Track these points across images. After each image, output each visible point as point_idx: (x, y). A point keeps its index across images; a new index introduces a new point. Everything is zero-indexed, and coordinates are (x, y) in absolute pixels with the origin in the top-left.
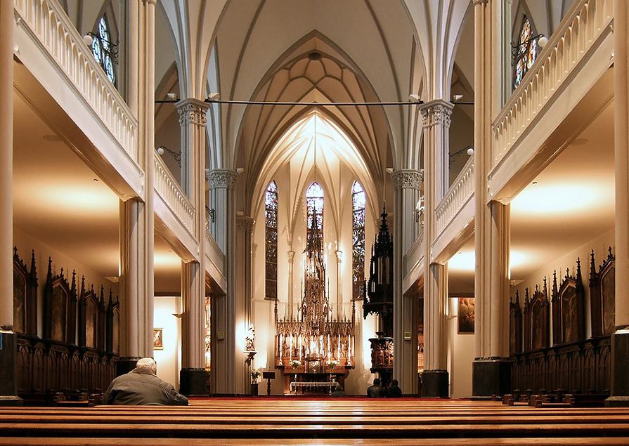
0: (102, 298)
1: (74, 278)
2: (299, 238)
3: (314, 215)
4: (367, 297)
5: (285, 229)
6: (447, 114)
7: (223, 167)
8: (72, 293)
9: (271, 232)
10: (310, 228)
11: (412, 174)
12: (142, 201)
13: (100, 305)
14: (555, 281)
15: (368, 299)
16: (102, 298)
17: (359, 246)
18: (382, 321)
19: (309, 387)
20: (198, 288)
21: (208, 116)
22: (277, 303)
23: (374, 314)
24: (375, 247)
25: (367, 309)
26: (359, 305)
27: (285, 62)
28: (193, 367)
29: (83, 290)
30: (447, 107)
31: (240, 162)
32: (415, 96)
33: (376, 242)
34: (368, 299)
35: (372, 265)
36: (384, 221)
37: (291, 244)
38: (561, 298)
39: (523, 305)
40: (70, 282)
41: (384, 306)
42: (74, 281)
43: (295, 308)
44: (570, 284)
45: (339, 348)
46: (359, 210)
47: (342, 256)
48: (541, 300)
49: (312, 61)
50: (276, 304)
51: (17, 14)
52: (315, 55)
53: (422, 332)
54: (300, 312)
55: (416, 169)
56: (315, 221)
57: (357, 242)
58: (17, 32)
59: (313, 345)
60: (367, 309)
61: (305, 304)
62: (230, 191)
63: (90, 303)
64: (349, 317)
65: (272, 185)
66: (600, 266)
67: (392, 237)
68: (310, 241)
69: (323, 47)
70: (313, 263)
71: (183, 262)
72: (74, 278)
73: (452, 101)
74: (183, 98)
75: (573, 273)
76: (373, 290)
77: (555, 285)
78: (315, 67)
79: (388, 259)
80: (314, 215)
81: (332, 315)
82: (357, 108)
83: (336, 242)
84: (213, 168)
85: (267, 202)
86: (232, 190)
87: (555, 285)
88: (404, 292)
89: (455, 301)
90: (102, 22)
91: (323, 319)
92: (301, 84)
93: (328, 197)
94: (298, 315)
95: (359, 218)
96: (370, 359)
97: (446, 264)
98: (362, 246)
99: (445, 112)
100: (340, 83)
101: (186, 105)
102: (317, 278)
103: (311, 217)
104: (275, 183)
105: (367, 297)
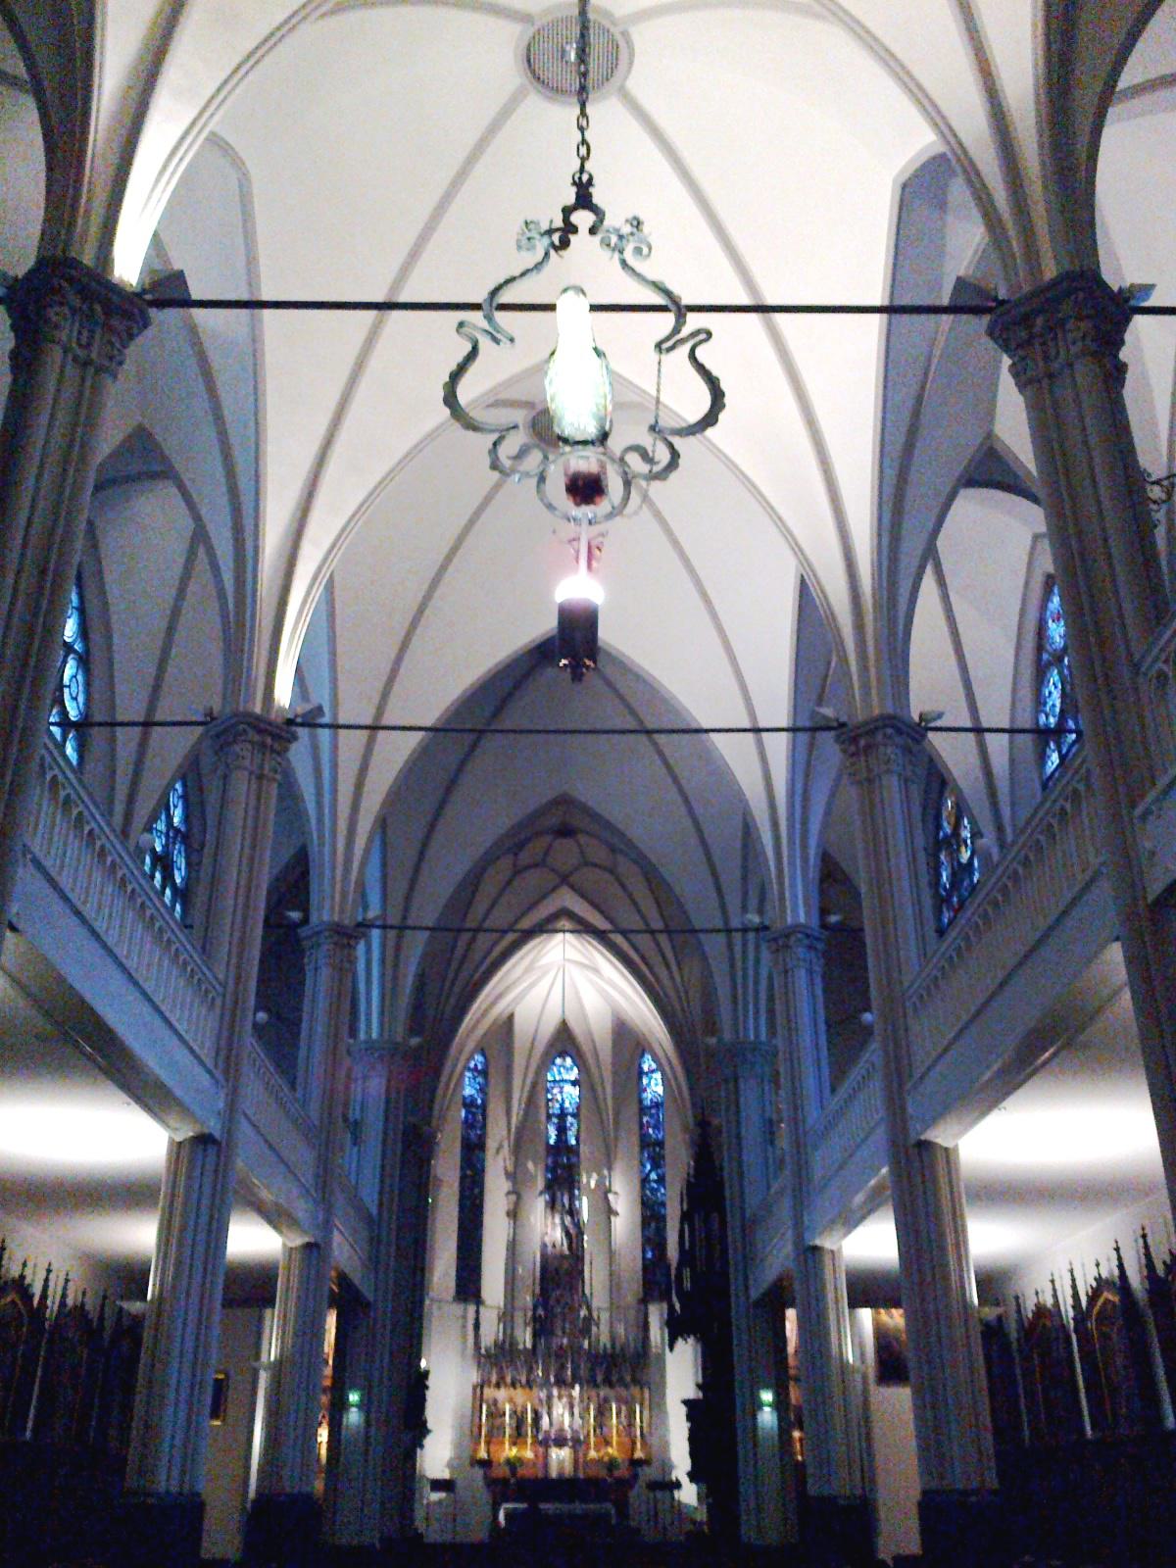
1: (47, 1280)
2: (530, 1165)
4: (675, 1299)
9: (473, 1151)
10: (552, 1142)
14: (1074, 1287)
15: (677, 1306)
21: (361, 947)
23: (691, 1340)
25: (676, 1329)
26: (656, 1315)
27: (514, 842)
29: (63, 1304)
31: (415, 1028)
32: (754, 918)
34: (677, 1306)
37: (511, 1176)
38: (1091, 1325)
40: (37, 1290)
43: (519, 1319)
44: (1107, 1295)
49: (558, 841)
50: (477, 1312)
51: (26, 849)
52: (566, 832)
55: (763, 1037)
56: (562, 1130)
58: (25, 879)
59: (560, 1409)
60: (676, 1329)
65: (479, 1058)
66: (1164, 1263)
68: (552, 1169)
69: (577, 821)
70: (557, 1220)
71: (284, 1245)
72: (47, 1280)
73: (824, 926)
74: (314, 919)
75: (1108, 1269)
76: (687, 1284)
77: (1076, 1296)
78: (565, 853)
81: (602, 1335)
82: (647, 925)
83: (606, 1172)
84: (362, 1036)
85: (468, 1091)
87: (1076, 1296)
88: (754, 1294)
89: (866, 1315)
90: (178, 786)
91: (581, 1347)
92: (533, 879)
94: (525, 1338)
97: (840, 1249)
98: (661, 1180)
99: (810, 947)
102: (567, 1252)
105: (675, 1299)
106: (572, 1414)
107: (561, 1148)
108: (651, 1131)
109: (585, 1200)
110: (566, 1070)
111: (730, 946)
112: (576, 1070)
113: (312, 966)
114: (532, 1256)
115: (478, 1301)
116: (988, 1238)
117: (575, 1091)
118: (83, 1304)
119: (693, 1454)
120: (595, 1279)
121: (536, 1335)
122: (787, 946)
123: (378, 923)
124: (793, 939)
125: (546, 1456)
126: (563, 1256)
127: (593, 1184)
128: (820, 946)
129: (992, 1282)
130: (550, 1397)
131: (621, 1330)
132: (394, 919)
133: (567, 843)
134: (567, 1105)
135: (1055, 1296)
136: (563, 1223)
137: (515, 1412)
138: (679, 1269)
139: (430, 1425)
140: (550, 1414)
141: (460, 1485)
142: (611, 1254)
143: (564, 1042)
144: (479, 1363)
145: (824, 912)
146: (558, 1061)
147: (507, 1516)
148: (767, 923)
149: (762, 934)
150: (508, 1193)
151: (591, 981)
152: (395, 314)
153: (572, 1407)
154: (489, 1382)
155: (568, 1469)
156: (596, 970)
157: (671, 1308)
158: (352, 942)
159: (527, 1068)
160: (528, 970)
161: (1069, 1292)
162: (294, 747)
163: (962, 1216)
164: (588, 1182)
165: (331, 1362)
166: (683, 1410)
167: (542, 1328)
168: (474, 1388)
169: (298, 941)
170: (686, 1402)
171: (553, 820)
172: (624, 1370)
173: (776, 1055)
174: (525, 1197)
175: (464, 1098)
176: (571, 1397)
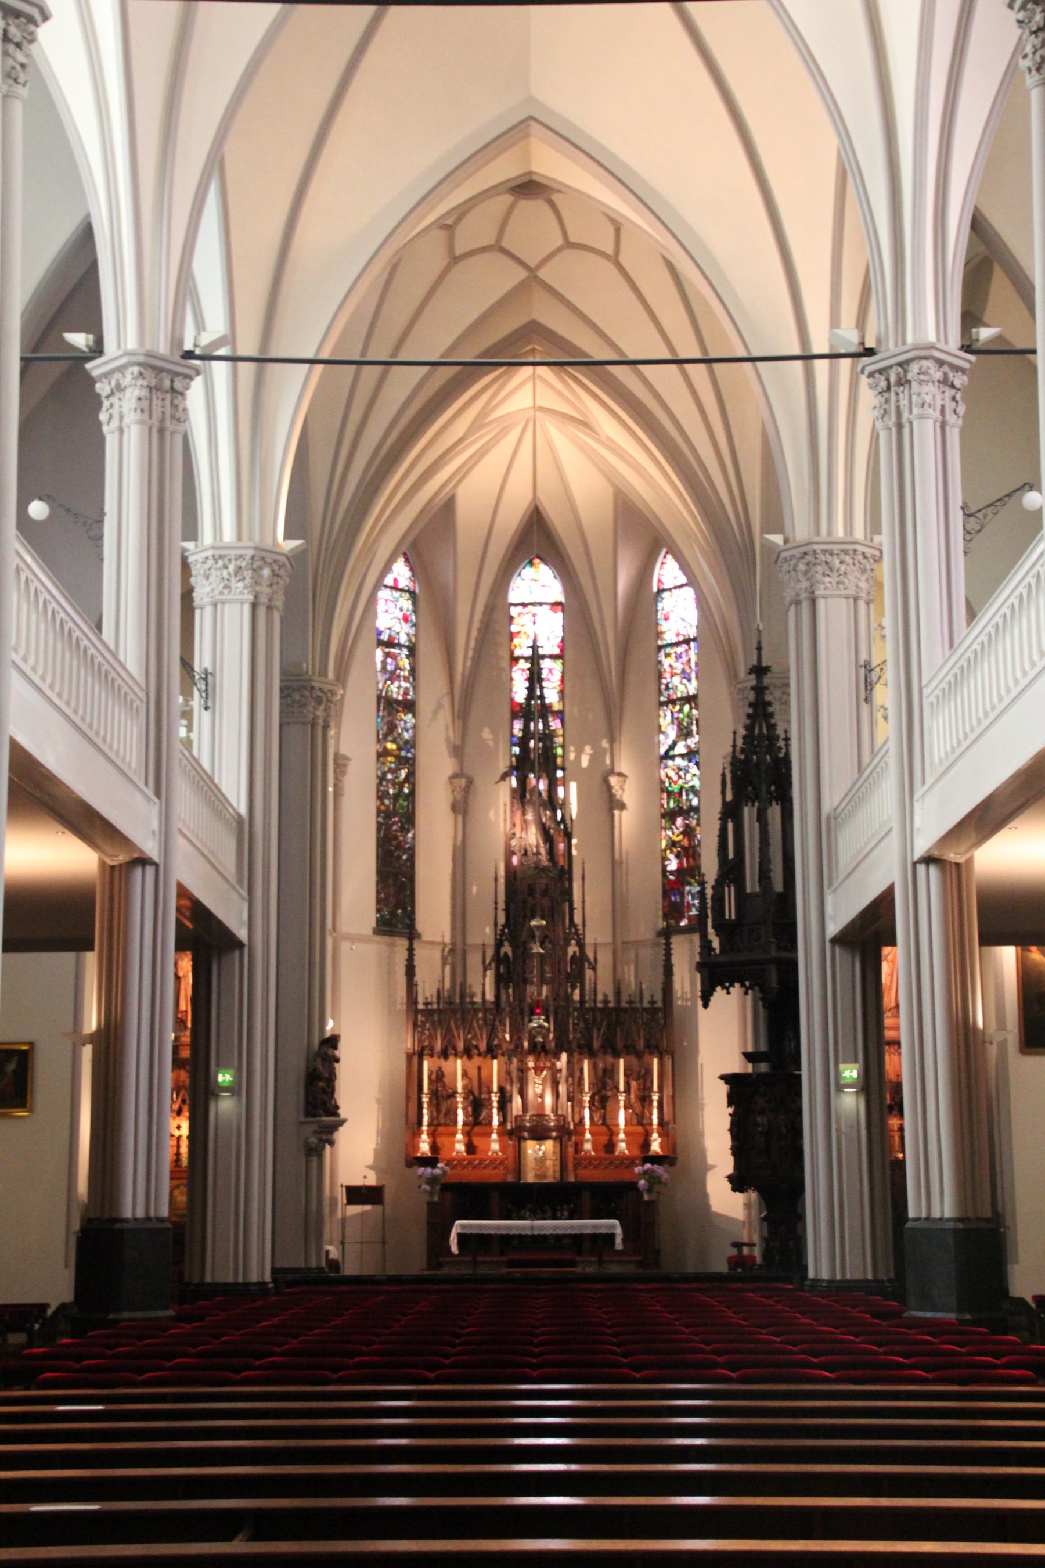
2: (487, 734)
4: (710, 930)
5: (440, 706)
6: (952, 386)
7: (239, 538)
11: (845, 552)
15: (716, 944)
17: (682, 756)
18: (761, 1009)
20: (150, 929)
22: (416, 944)
23: (736, 990)
26: (685, 954)
28: (128, 1214)
34: (716, 944)
35: (723, 830)
36: (759, 690)
43: (474, 961)
45: (622, 1098)
46: (678, 644)
47: (627, 787)
50: (411, 950)
53: (897, 1043)
54: (490, 975)
55: (859, 534)
59: (536, 1086)
60: (714, 975)
62: (262, 612)
64: (652, 989)
67: (787, 739)
69: (549, 163)
70: (530, 817)
71: (102, 864)
76: (730, 912)
79: (775, 812)
80: (535, 659)
81: (601, 982)
83: (605, 744)
86: (270, 608)
89: (1007, 955)
91: (568, 998)
93: (576, 608)
94: (483, 986)
95: (679, 666)
96: (727, 1141)
97: (970, 861)
99: (945, 382)
100: (610, 267)
101: (121, 369)
104: (407, 560)
105: (710, 930)
106: (557, 1095)
107: (533, 709)
109: (573, 786)
110: (537, 585)
111: (809, 378)
113: (115, 423)
114: (490, 868)
115: (412, 934)
119: (737, 1151)
120: (590, 901)
121: (500, 981)
122: (903, 382)
123: (222, 352)
124: (914, 368)
125: (519, 1155)
126: (539, 868)
127: (585, 762)
128: (959, 380)
130: (523, 1070)
131: (630, 976)
132: (248, 346)
133: (533, 208)
136: (538, 817)
137: (471, 1092)
138: (719, 886)
139: (343, 1113)
140: (522, 1093)
141: (388, 1196)
142: (615, 866)
143: (536, 538)
144: (415, 1025)
145: (971, 318)
147: (460, 1236)
148: (870, 344)
150: (454, 776)
151: (582, 448)
152: (394, 368)
153: (555, 1084)
154: (432, 1049)
155: (552, 1174)
156: (585, 425)
157: (706, 945)
158: (178, 385)
160: (475, 427)
162: (44, 32)
164: (578, 758)
165: (189, 1025)
166: (723, 1088)
167: (509, 971)
168: (409, 1057)
169: (91, 381)
170: (726, 1078)
172: (638, 1033)
173: (878, 560)
174: (478, 782)
176: (555, 1072)
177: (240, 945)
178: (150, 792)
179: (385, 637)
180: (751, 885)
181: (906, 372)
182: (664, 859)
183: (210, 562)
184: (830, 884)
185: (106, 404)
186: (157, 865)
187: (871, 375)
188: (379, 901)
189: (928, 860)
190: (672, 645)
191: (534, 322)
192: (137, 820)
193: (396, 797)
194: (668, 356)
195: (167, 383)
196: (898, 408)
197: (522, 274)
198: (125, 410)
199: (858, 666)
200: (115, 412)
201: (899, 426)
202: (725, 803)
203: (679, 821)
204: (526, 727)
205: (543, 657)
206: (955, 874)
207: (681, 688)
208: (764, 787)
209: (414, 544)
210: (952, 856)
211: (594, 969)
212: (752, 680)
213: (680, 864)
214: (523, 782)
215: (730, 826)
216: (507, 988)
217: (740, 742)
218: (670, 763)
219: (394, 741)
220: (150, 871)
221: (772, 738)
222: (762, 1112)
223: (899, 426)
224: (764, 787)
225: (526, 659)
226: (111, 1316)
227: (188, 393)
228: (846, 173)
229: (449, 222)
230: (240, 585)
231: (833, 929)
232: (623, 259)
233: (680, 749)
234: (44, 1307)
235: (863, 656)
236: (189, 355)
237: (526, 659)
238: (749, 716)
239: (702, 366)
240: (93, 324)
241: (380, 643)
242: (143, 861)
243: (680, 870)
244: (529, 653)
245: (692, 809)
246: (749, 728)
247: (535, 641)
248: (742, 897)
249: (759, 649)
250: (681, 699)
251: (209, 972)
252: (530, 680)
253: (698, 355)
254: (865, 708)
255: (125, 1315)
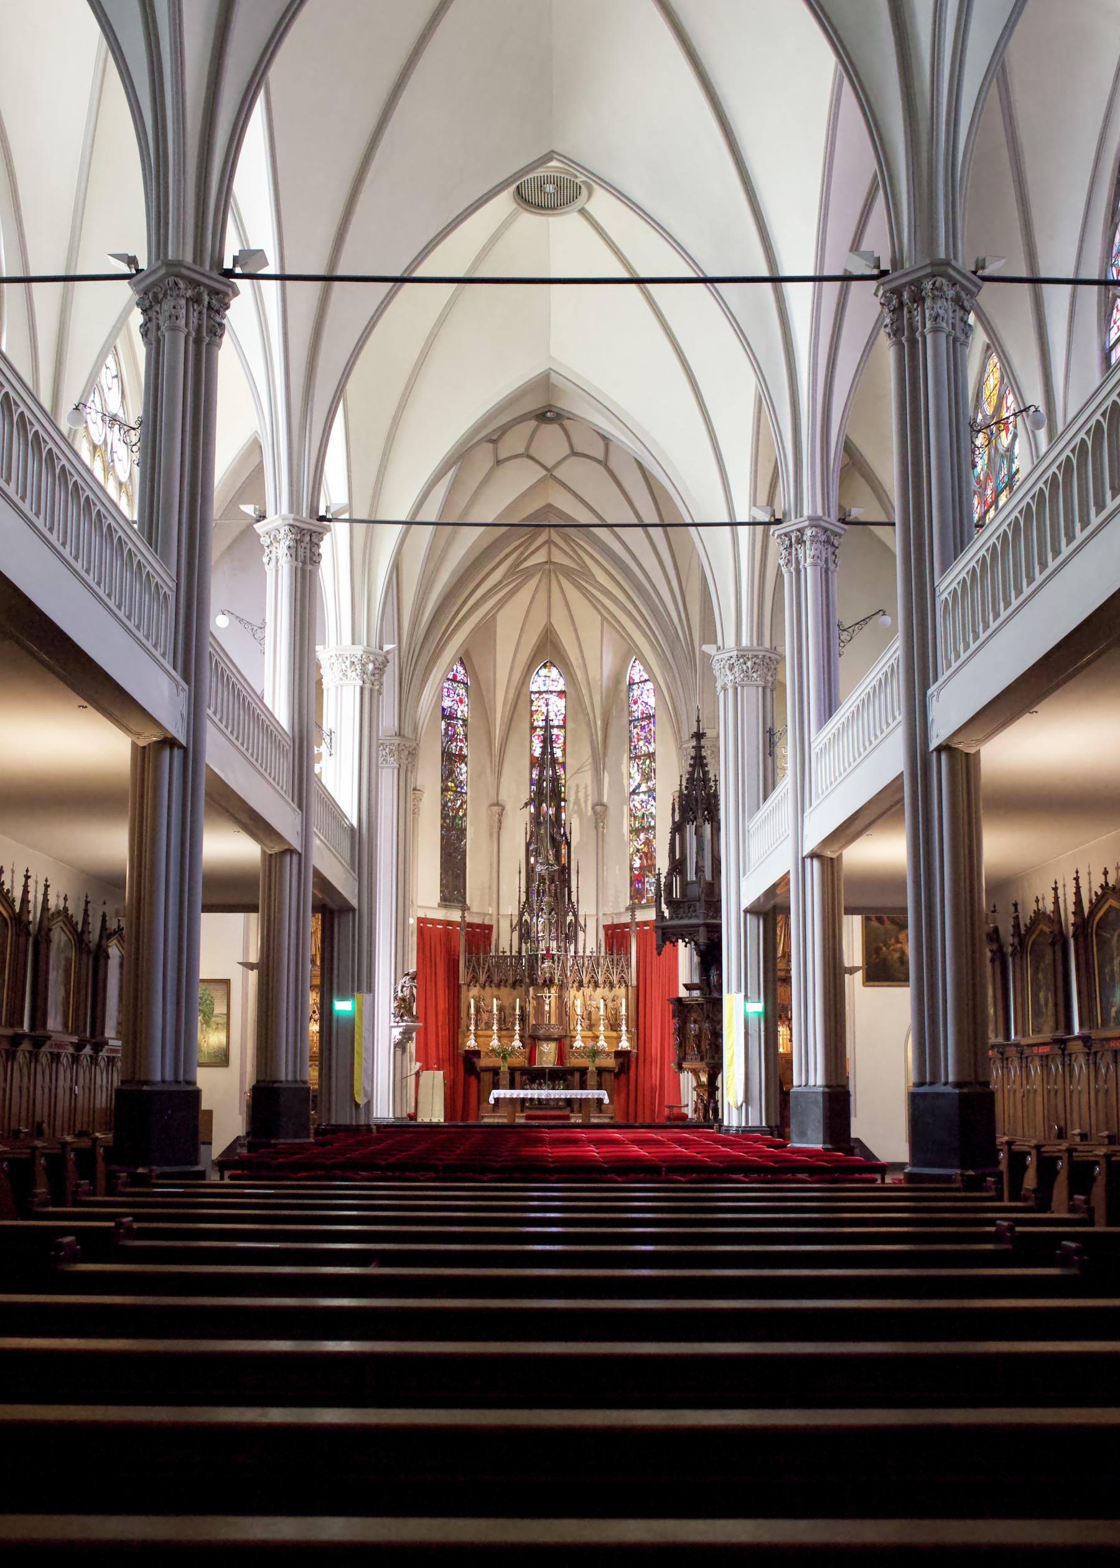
0: (85, 922)
1: (26, 886)
3: (548, 727)
4: (664, 906)
8: (19, 920)
10: (537, 753)
12: (180, 746)
13: (79, 938)
16: (85, 922)
17: (644, 793)
19: (532, 1099)
20: (296, 900)
24: (680, 805)
28: (283, 1078)
30: (832, 531)
33: (681, 791)
34: (667, 914)
35: (673, 840)
36: (698, 748)
39: (1008, 938)
40: (18, 894)
41: (702, 929)
42: (26, 891)
46: (643, 719)
48: (1047, 930)
54: (516, 934)
56: (548, 741)
57: (639, 786)
61: (526, 917)
63: (59, 936)
67: (716, 781)
71: (263, 852)
76: (677, 894)
77: (1078, 902)
80: (548, 727)
97: (840, 857)
100: (600, 469)
103: (539, 732)
105: (664, 906)
108: (647, 698)
112: (562, 681)
116: (1000, 846)
117: (561, 703)
118: (66, 909)
129: (1003, 885)
133: (550, 431)
134: (552, 716)
135: (1056, 902)
146: (543, 672)
148: (779, 516)
149: (773, 528)
159: (509, 681)
161: (1071, 899)
163: (978, 820)
171: (532, 404)
175: (444, 709)
177: (352, 909)
178: (295, 806)
179: (447, 713)
180: (691, 876)
181: (802, 535)
182: (632, 860)
183: (334, 658)
184: (744, 874)
185: (267, 551)
186: (300, 854)
187: (779, 536)
188: (441, 885)
189: (813, 855)
190: (638, 719)
191: (549, 506)
192: (283, 818)
193: (454, 817)
194: (636, 522)
195: (307, 538)
196: (797, 558)
197: (544, 473)
198: (280, 555)
199: (764, 732)
200: (273, 556)
201: (798, 571)
202: (674, 822)
203: (642, 836)
204: (541, 772)
205: (553, 727)
206: (830, 866)
207: (644, 748)
208: (700, 812)
209: (467, 652)
210: (829, 854)
211: (584, 931)
212: (694, 743)
213: (642, 864)
214: (538, 809)
215: (677, 837)
216: (526, 943)
217: (684, 783)
218: (636, 797)
219: (452, 781)
220: (177, 753)
221: (705, 780)
222: (695, 1022)
223: (798, 571)
224: (700, 812)
225: (541, 728)
226: (273, 1141)
227: (321, 543)
228: (763, 402)
229: (494, 437)
230: (354, 674)
231: (746, 903)
232: (612, 464)
233: (643, 788)
234: (238, 1138)
235: (769, 725)
236: (322, 519)
237: (541, 728)
238: (691, 765)
239: (660, 529)
240: (259, 498)
241: (444, 717)
242: (291, 851)
243: (642, 867)
244: (542, 724)
245: (650, 827)
246: (691, 774)
247: (547, 716)
248: (685, 884)
249: (698, 721)
250: (645, 755)
251: (332, 925)
252: (544, 741)
253: (657, 521)
254: (769, 759)
255: (282, 1141)
